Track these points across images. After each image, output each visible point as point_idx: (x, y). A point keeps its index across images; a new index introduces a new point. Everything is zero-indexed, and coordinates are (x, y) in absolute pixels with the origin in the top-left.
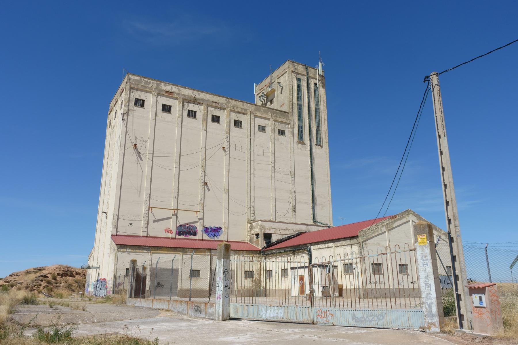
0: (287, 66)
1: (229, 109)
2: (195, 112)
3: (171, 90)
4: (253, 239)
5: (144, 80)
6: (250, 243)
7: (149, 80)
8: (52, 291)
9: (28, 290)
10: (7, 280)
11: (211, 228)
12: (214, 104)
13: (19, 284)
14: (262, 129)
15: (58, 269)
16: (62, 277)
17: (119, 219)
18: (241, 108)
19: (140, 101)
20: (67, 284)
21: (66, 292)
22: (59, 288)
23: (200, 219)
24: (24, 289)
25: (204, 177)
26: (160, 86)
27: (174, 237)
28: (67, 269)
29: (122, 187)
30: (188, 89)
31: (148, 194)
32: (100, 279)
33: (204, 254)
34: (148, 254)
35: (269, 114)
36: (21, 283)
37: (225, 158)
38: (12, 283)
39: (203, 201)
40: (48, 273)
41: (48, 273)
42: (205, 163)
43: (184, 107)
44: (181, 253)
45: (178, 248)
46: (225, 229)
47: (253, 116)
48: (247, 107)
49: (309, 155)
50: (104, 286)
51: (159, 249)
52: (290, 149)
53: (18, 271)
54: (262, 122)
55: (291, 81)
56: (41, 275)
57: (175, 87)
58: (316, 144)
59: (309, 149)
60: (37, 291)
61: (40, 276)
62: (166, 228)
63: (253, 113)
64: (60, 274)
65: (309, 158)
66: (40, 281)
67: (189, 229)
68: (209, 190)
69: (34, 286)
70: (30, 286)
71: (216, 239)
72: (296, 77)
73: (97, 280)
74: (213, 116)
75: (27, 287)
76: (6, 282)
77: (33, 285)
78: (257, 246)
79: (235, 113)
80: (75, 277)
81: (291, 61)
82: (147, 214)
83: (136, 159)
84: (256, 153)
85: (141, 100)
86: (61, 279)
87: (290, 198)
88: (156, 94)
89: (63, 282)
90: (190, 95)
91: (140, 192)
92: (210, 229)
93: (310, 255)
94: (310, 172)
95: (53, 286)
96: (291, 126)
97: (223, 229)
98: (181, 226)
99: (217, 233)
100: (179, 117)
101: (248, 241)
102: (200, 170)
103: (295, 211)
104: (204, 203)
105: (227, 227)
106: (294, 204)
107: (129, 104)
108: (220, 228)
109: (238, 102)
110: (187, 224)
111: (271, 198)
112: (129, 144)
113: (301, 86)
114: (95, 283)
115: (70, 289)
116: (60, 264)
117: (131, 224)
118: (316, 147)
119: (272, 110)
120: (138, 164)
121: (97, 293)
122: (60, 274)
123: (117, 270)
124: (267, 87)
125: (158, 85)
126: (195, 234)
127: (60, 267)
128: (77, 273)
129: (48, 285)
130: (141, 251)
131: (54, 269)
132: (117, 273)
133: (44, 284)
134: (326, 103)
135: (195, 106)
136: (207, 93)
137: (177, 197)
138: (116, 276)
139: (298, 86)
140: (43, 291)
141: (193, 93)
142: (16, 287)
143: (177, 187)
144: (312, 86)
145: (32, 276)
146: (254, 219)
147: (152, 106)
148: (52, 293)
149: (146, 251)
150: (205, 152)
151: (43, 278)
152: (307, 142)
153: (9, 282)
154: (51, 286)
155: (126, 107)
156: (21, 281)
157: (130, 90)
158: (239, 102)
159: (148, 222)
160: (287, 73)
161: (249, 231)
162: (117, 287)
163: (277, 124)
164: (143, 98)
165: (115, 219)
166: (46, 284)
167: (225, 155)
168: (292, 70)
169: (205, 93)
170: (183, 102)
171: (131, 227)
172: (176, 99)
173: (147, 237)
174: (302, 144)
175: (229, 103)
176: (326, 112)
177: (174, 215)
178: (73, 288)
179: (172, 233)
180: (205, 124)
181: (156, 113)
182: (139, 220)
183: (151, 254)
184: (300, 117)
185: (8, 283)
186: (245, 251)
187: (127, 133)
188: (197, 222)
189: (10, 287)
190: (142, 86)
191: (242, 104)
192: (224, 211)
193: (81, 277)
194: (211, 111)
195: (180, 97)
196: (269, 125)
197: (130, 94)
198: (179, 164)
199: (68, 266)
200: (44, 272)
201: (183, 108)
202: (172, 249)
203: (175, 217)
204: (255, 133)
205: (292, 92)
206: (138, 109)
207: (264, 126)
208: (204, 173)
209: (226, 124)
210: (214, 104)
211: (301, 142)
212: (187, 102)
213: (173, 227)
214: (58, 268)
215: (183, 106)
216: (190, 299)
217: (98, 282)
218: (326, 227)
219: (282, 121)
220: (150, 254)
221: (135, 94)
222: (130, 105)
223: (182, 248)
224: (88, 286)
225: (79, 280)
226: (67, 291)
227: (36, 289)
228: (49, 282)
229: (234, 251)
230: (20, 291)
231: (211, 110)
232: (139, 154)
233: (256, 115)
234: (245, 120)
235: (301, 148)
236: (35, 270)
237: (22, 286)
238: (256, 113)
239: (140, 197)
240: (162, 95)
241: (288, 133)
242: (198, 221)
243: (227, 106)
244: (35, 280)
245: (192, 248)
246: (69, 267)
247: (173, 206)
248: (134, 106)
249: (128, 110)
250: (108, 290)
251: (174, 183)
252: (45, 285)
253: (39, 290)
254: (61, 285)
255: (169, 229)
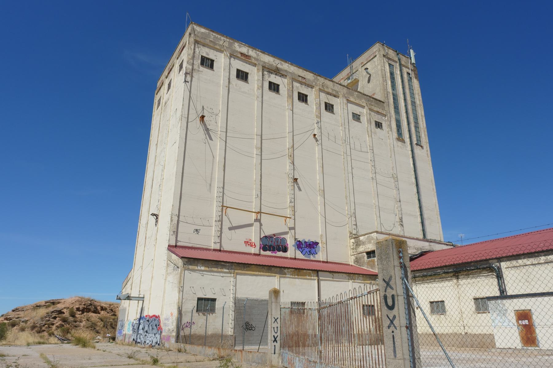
0: (376, 48)
1: (317, 88)
2: (278, 85)
3: (247, 53)
4: (362, 260)
5: (212, 34)
6: (357, 265)
7: (219, 36)
8: (68, 332)
9: (34, 331)
10: (9, 317)
11: (305, 242)
12: (300, 79)
13: (23, 322)
14: (357, 117)
15: (78, 303)
16: (83, 313)
17: (180, 222)
18: (332, 89)
19: (208, 60)
20: (89, 322)
21: (88, 335)
22: (78, 328)
23: (290, 229)
24: (29, 329)
25: (293, 171)
26: (233, 45)
27: (258, 252)
28: (90, 303)
29: (184, 174)
30: (269, 55)
31: (221, 188)
32: (146, 316)
33: (309, 277)
34: (229, 275)
35: (362, 100)
36: (26, 322)
37: (317, 149)
38: (13, 320)
39: (293, 203)
40: (65, 308)
41: (65, 308)
42: (293, 152)
43: (264, 77)
44: (278, 276)
45: (274, 266)
46: (323, 245)
47: (346, 100)
48: (338, 88)
49: (411, 156)
50: (155, 327)
51: (247, 267)
52: (389, 146)
53: (25, 305)
54: (357, 110)
55: (383, 65)
56: (54, 311)
57: (252, 51)
58: (416, 144)
59: (409, 148)
60: (47, 332)
61: (53, 312)
62: (246, 239)
63: (346, 97)
64: (80, 309)
65: (411, 160)
66: (52, 318)
67: (277, 242)
68: (300, 190)
69: (44, 326)
70: (38, 325)
71: (312, 258)
72: (388, 63)
73: (138, 317)
74: (299, 93)
75: (33, 327)
76: (6, 319)
77: (41, 325)
78: (372, 269)
79: (325, 94)
80: (99, 313)
81: (381, 44)
82: (220, 216)
83: (204, 137)
84: (352, 146)
85: (208, 59)
86: (81, 315)
87: (396, 208)
88: (229, 55)
89: (85, 321)
90: (271, 63)
91: (210, 185)
92: (303, 243)
93: (500, 277)
94: (413, 176)
95: (71, 326)
96: (388, 119)
97: (320, 245)
98: (266, 237)
99: (313, 250)
100: (258, 89)
101: (352, 263)
102: (288, 162)
103: (402, 225)
104: (294, 206)
105: (325, 242)
106: (400, 216)
107: (193, 61)
108: (317, 244)
109: (327, 81)
110: (274, 235)
111: (374, 206)
112: (193, 116)
113: (394, 74)
114: (135, 322)
115: (93, 330)
116: (80, 296)
117: (197, 230)
118: (416, 147)
119: (365, 96)
120: (207, 144)
121: (140, 338)
122: (80, 309)
123: (184, 301)
124: (345, 80)
125: (231, 45)
126: (285, 250)
127: (80, 299)
128: (103, 309)
129: (63, 323)
130: (220, 270)
131: (73, 302)
132: (183, 305)
133: (58, 322)
134: (421, 96)
135: (278, 77)
136: (291, 64)
137: (259, 195)
138: (181, 310)
139: (391, 73)
140: (56, 333)
141: (274, 61)
142: (19, 326)
143: (260, 181)
144: (405, 75)
145: (42, 312)
146: (357, 233)
147: (224, 70)
148: (69, 336)
149: (227, 271)
150: (292, 138)
151: (57, 314)
152: (407, 140)
153: (10, 319)
154: (68, 326)
155: (189, 65)
156: (27, 319)
157: (195, 45)
158: (329, 81)
159: (221, 228)
160: (378, 56)
161: (353, 249)
162: (183, 329)
163: (372, 114)
164: (211, 56)
165: (173, 221)
166: (60, 322)
167: (317, 144)
168: (383, 53)
169: (288, 63)
170: (263, 70)
171: (197, 235)
172: (253, 66)
173: (220, 251)
174: (402, 142)
175: (317, 81)
176: (422, 106)
177: (256, 220)
178: (98, 329)
179: (254, 246)
180: (290, 102)
181: (229, 79)
182: (208, 224)
183: (235, 274)
184: (396, 108)
185: (8, 321)
186: (361, 276)
187: (191, 100)
188: (286, 233)
189: (11, 327)
190: (211, 41)
191: (332, 84)
192: (320, 219)
193: (108, 313)
194: (297, 87)
195: (259, 64)
196: (364, 115)
197: (194, 49)
198: (260, 150)
199: (91, 299)
200: (59, 307)
201: (263, 78)
202: (265, 269)
203: (258, 223)
204: (349, 121)
205: (385, 79)
206: (205, 70)
207: (359, 114)
208: (293, 166)
209: (316, 105)
210: (300, 79)
211: (401, 139)
212: (267, 72)
213: (255, 239)
214: (78, 301)
215: (263, 75)
216: (243, 348)
217: (141, 321)
218: (451, 245)
219: (378, 111)
220: (232, 275)
221: (201, 50)
222: (195, 63)
223: (279, 267)
224: (122, 326)
225: (105, 318)
226: (90, 333)
227: (46, 330)
228: (65, 320)
229: (347, 274)
230: (24, 332)
231: (297, 86)
232: (207, 130)
233: (349, 99)
234: (338, 103)
235: (401, 147)
236: (47, 304)
237: (26, 325)
238: (349, 98)
239: (210, 192)
240: (236, 57)
241: (386, 126)
242: (288, 232)
243: (316, 83)
244: (46, 317)
245: (292, 268)
246: (92, 300)
247: (254, 207)
248: (200, 65)
249: (193, 69)
250: (163, 334)
251: (255, 175)
252: (59, 325)
253: (50, 332)
254: (82, 324)
255: (250, 240)
